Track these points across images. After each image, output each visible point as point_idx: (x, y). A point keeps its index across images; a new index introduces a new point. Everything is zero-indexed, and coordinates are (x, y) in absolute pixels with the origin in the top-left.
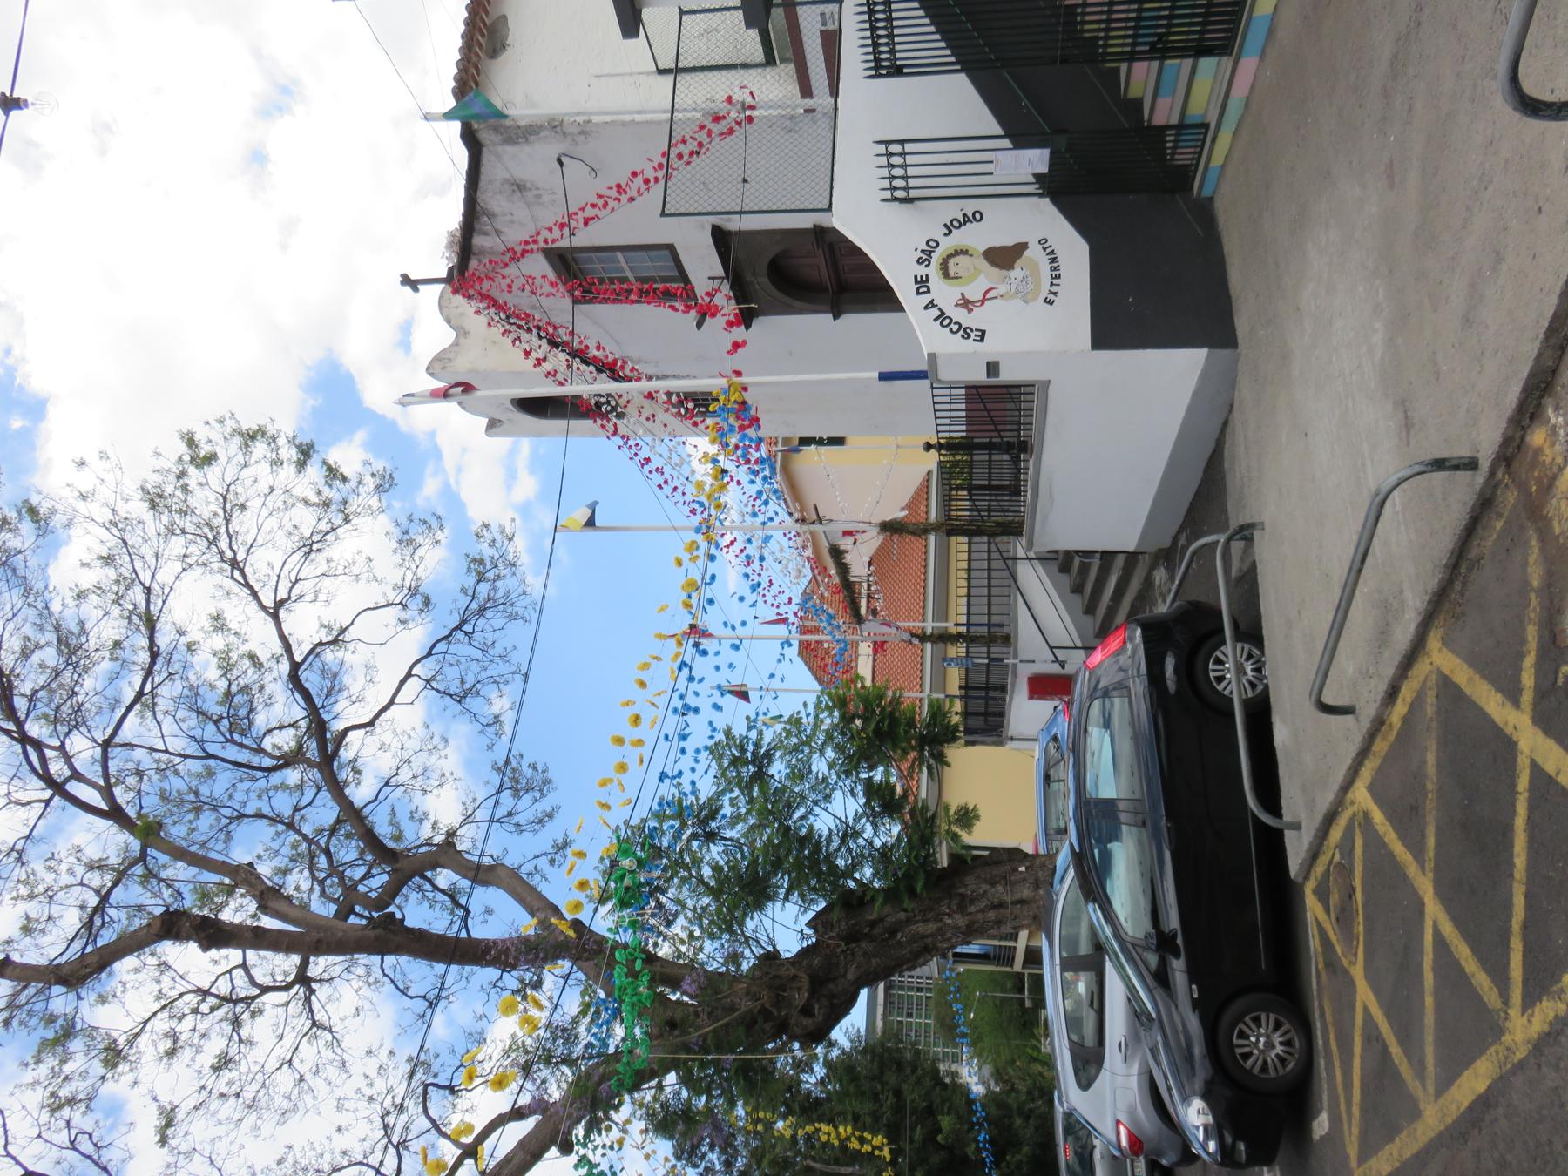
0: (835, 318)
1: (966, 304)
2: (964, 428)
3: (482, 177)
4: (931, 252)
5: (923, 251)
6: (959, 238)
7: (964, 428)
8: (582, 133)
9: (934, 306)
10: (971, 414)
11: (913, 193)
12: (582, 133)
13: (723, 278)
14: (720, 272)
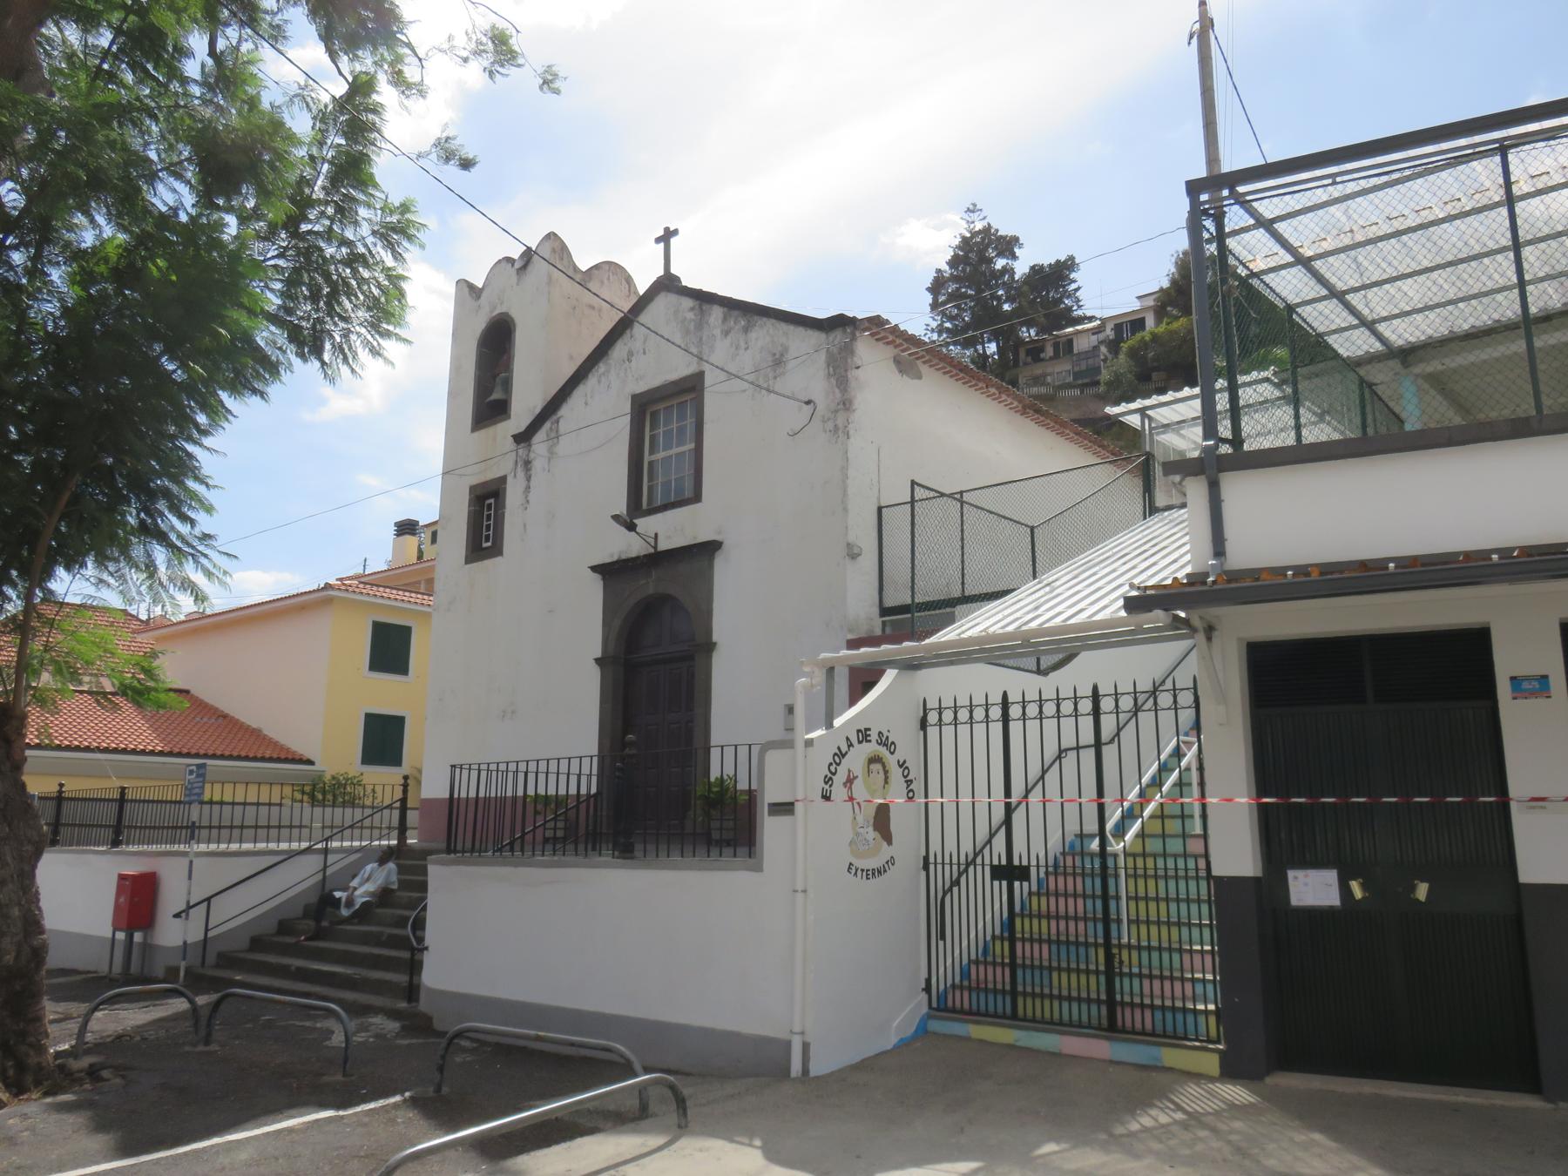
0: (597, 660)
1: (850, 781)
2: (531, 792)
3: (792, 327)
4: (886, 745)
5: (887, 738)
6: (896, 773)
7: (531, 792)
8: (836, 428)
9: (849, 746)
11: (933, 732)
12: (836, 428)
14: (663, 545)
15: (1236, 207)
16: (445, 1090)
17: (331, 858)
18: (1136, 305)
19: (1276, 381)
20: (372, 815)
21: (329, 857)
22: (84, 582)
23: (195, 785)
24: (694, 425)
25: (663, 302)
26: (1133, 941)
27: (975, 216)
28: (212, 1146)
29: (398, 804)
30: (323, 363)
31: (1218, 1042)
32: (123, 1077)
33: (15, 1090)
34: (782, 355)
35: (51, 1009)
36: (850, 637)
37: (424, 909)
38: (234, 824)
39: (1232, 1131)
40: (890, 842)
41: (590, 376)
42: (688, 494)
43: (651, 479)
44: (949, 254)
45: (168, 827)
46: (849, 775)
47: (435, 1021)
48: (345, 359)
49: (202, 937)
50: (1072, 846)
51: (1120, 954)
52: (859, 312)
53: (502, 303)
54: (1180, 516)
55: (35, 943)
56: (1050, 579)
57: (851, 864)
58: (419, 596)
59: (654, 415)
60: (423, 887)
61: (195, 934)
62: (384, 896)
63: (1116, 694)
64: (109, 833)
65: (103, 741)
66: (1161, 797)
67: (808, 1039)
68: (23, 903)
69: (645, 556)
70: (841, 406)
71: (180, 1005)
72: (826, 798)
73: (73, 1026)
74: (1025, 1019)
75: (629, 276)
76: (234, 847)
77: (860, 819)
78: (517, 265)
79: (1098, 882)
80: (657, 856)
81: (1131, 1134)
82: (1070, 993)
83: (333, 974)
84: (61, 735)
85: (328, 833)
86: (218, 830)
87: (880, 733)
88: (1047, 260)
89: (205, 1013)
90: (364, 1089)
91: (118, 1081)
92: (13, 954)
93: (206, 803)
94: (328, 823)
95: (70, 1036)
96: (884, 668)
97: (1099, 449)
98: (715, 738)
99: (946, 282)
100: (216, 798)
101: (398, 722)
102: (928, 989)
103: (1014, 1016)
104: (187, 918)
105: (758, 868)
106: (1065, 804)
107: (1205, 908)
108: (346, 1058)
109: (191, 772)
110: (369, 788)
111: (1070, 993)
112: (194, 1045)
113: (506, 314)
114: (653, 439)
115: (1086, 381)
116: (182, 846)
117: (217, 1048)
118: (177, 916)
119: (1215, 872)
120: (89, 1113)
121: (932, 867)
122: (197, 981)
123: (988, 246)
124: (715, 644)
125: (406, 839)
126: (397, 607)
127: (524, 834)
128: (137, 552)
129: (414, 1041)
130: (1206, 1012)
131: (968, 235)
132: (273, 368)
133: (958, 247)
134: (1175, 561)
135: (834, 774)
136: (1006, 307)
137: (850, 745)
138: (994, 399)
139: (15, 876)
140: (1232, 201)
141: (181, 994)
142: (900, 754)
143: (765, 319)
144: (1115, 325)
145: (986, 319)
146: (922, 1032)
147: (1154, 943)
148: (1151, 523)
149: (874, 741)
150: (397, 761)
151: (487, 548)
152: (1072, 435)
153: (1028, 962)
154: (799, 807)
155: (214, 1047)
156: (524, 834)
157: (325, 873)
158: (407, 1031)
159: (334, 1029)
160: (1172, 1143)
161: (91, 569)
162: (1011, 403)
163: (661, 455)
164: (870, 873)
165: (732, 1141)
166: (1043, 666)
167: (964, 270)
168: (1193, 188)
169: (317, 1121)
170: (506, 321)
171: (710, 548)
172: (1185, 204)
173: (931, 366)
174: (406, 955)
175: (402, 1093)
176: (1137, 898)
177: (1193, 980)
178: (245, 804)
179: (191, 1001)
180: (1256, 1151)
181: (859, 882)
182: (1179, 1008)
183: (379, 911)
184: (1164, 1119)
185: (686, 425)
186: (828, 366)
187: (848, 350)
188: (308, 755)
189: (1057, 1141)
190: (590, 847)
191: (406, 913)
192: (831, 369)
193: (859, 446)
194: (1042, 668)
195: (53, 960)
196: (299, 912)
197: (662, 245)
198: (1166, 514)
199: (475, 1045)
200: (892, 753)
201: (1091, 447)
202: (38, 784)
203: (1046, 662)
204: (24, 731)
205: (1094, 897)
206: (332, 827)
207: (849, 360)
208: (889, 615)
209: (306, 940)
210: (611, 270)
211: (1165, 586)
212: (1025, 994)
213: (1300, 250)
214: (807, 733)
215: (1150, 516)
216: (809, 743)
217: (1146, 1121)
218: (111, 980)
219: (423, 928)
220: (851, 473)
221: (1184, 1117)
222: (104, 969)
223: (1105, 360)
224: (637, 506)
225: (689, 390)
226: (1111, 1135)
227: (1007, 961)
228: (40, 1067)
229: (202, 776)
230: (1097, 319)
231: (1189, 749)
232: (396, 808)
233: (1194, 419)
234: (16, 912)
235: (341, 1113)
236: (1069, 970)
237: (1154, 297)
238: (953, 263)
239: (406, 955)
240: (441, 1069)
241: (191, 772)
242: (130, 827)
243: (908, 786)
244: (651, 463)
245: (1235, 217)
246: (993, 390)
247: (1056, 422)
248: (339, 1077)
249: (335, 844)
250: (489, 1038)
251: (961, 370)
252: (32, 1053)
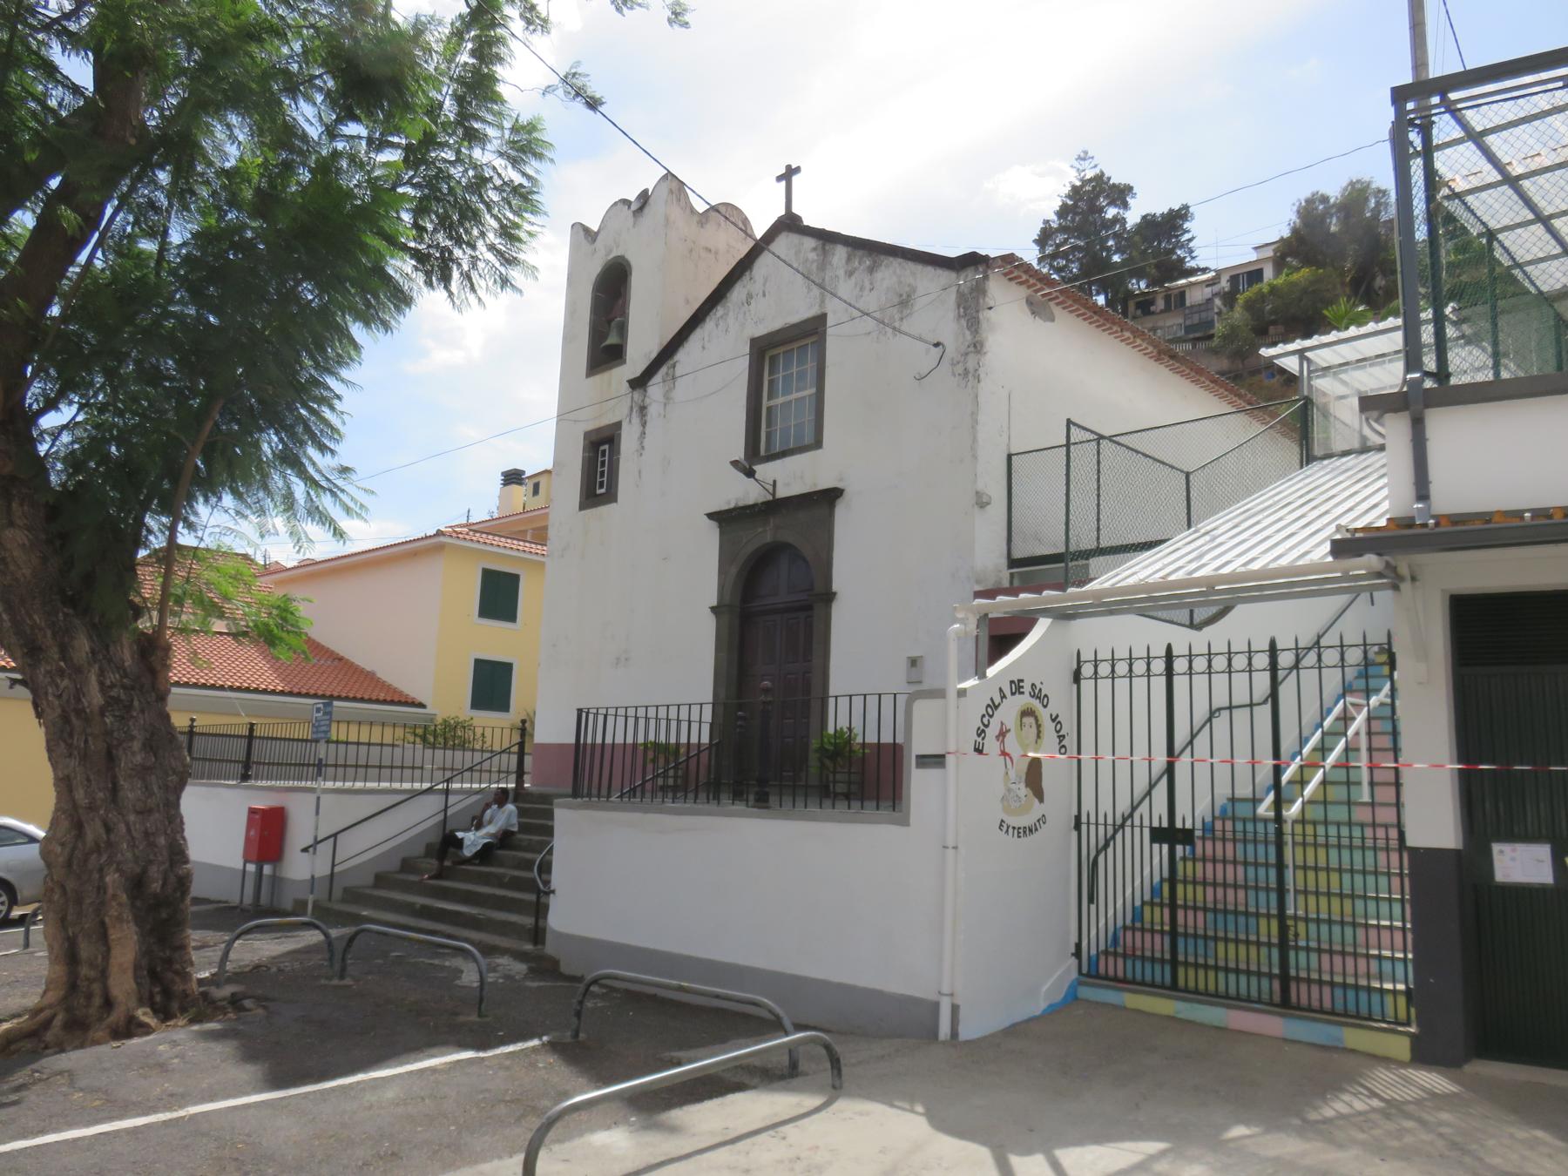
0: (713, 609)
1: (1002, 734)
2: (609, 740)
5: (1040, 690)
6: (1049, 727)
8: (966, 372)
9: (1002, 698)
10: (589, 749)
11: (1088, 686)
12: (966, 372)
13: (774, 494)
14: (782, 493)
15: (1447, 117)
16: (582, 1036)
17: (452, 799)
18: (1253, 257)
19: (1455, 318)
20: (491, 758)
21: (450, 797)
22: (223, 514)
23: (323, 723)
24: (815, 368)
25: (783, 244)
26: (1301, 913)
27: (1086, 164)
28: (358, 1083)
29: (515, 749)
30: (451, 294)
31: (1408, 1024)
32: (264, 1007)
33: (162, 1016)
34: (909, 296)
35: (195, 936)
36: (978, 588)
37: (550, 852)
38: (359, 763)
39: (1441, 1124)
40: (1041, 800)
41: (708, 320)
42: (808, 439)
43: (769, 425)
44: (1056, 204)
45: (295, 765)
46: (1002, 729)
47: (562, 964)
48: (473, 289)
49: (329, 872)
50: (1224, 810)
51: (1296, 926)
52: (992, 248)
53: (618, 247)
54: (1343, 464)
55: (180, 872)
56: (1208, 528)
57: (1002, 821)
58: (527, 544)
59: (773, 360)
60: (549, 831)
61: (323, 870)
62: (505, 839)
63: (1250, 652)
64: (239, 768)
65: (228, 680)
66: (1302, 760)
67: (958, 1001)
68: (169, 832)
69: (763, 503)
70: (972, 349)
71: (313, 937)
72: (979, 751)
73: (215, 954)
74: (1186, 990)
75: (746, 218)
76: (359, 785)
77: (1012, 774)
78: (634, 207)
79: (1272, 850)
80: (781, 806)
81: (1326, 1121)
82: (1237, 965)
83: (458, 913)
84: (188, 672)
85: (448, 774)
86: (344, 768)
87: (1033, 685)
88: (1160, 208)
89: (339, 948)
90: (501, 1030)
91: (260, 1011)
92: (160, 882)
93: (333, 742)
94: (448, 765)
95: (210, 964)
96: (1036, 616)
97: (1234, 399)
98: (833, 690)
99: (1053, 233)
100: (342, 737)
101: (507, 668)
102: (1078, 953)
103: (1174, 986)
104: (314, 853)
105: (905, 822)
106: (1195, 763)
107: (1396, 881)
108: (480, 998)
109: (318, 710)
110: (479, 731)
111: (1237, 965)
112: (330, 978)
113: (622, 257)
114: (771, 382)
115: (1197, 335)
116: (309, 783)
117: (351, 983)
118: (305, 850)
119: (1411, 841)
120: (235, 1043)
121: (1084, 827)
122: (325, 915)
123: (1097, 197)
124: (835, 594)
125: (523, 782)
126: (507, 554)
127: (644, 782)
128: (277, 480)
129: (542, 984)
130: (1395, 992)
131: (1078, 183)
132: (402, 299)
133: (1068, 196)
134: (1350, 509)
135: (987, 726)
136: (1116, 258)
137: (1003, 697)
138: (1128, 344)
139: (161, 805)
140: (1443, 110)
141: (317, 927)
142: (1053, 708)
143: (891, 259)
144: (1231, 277)
145: (1095, 271)
146: (1072, 998)
147: (1324, 916)
148: (1308, 473)
149: (1027, 694)
150: (503, 705)
151: (601, 495)
152: (1207, 383)
153: (1191, 931)
154: (950, 760)
155: (348, 981)
156: (644, 782)
157: (446, 814)
158: (535, 972)
159: (462, 968)
160: (1376, 1132)
161: (228, 500)
162: (1146, 348)
163: (780, 400)
164: (1021, 831)
165: (892, 1106)
166: (1197, 620)
167: (1073, 220)
168: (1399, 95)
169: (458, 1061)
170: (621, 264)
171: (831, 496)
172: (1389, 113)
173: (1064, 308)
174: (532, 897)
175: (540, 1038)
176: (1305, 868)
177: (1380, 957)
178: (369, 744)
179: (326, 935)
180: (1474, 1147)
181: (1011, 840)
182: (1363, 987)
183: (500, 852)
184: (1359, 1105)
185: (792, 374)
186: (959, 308)
187: (979, 290)
188: (420, 698)
189: (1247, 1123)
190: (711, 797)
191: (529, 856)
192: (962, 310)
193: (990, 389)
194: (1195, 623)
195: (197, 889)
196: (419, 850)
197: (783, 183)
198: (1326, 462)
199: (604, 991)
200: (1045, 706)
201: (1226, 396)
202: (179, 721)
203: (1201, 614)
204: (168, 662)
205: (1267, 865)
206: (452, 769)
207: (981, 301)
208: (1018, 567)
209: (430, 878)
210: (727, 214)
211: (1378, 529)
212: (1186, 964)
213: (1508, 167)
214: (960, 682)
215: (1307, 464)
216: (962, 693)
217: (1340, 1107)
218: (242, 910)
219: (549, 871)
220: (981, 418)
221: (1382, 1104)
222: (234, 899)
223: (1219, 314)
224: (754, 455)
225: (811, 332)
226: (1305, 1120)
227: (1167, 928)
228: (185, 995)
229: (330, 713)
230: (1210, 270)
231: (1359, 713)
232: (514, 753)
233: (1397, 352)
234: (162, 841)
235: (482, 1054)
236: (1226, 940)
237: (1273, 247)
238: (1063, 212)
239: (533, 897)
240: (578, 1014)
241: (318, 710)
242: (258, 763)
243: (1060, 741)
244: (769, 409)
245: (1444, 129)
246: (1127, 334)
247: (1192, 370)
248: (474, 1018)
249: (456, 786)
250: (617, 984)
251: (1095, 313)
252: (177, 979)
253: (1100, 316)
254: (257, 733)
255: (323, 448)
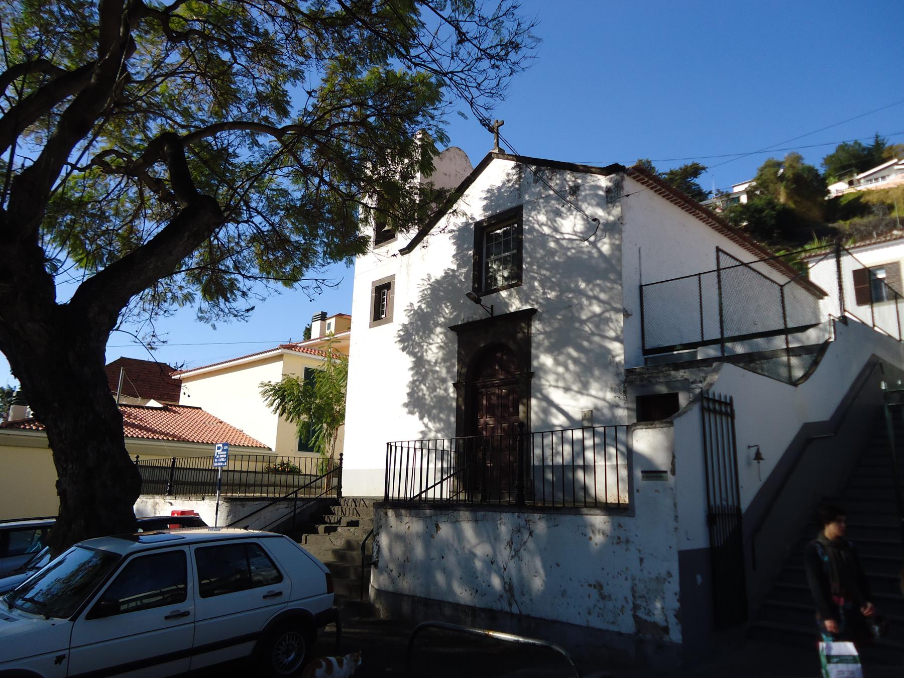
13: (492, 314)
114: (487, 248)
247: (740, 237)
253: (689, 204)
254: (177, 465)
255: (227, 300)
